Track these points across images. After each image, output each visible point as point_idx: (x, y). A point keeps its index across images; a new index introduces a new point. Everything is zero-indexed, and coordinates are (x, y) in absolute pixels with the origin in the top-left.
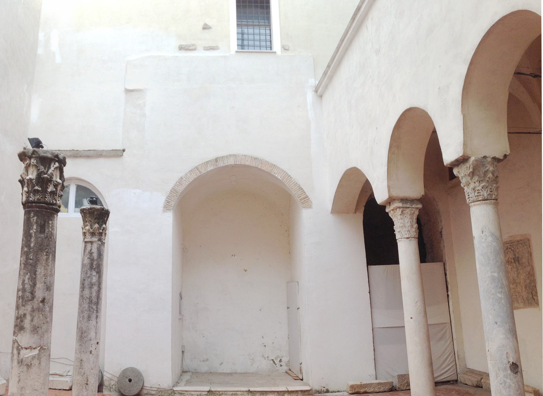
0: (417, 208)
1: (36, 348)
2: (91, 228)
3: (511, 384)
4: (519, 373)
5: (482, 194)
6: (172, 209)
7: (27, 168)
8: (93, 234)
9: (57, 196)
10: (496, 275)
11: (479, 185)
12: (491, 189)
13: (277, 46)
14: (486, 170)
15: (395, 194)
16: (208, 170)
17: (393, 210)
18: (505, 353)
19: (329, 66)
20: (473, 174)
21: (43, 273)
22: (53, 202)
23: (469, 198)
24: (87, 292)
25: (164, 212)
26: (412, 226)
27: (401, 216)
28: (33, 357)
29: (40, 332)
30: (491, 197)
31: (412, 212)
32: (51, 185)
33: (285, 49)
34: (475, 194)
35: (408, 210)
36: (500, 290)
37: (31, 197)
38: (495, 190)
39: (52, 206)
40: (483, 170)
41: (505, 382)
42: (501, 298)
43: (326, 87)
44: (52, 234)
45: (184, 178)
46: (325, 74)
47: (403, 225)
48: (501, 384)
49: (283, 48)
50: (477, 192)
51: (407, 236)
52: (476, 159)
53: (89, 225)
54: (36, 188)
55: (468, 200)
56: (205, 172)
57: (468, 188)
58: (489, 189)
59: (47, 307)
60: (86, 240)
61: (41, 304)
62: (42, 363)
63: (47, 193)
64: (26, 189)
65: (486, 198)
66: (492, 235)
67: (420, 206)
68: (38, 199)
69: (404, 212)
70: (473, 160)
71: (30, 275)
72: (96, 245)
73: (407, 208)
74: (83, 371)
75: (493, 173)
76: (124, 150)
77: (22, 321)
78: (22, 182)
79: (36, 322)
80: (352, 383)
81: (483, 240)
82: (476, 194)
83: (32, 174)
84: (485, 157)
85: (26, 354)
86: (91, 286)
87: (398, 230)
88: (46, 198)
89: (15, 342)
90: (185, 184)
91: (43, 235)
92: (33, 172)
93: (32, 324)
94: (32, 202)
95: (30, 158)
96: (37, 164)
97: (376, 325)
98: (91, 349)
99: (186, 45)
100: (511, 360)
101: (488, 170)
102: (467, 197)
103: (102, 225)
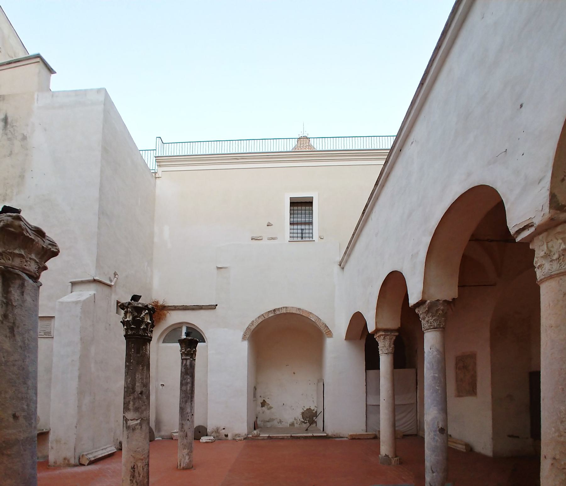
0: (395, 335)
1: (138, 419)
2: (186, 351)
3: (438, 439)
4: (445, 434)
5: (433, 324)
6: (248, 339)
7: (126, 314)
8: (187, 355)
9: (148, 331)
10: (437, 375)
11: (432, 318)
12: (440, 321)
13: (316, 237)
14: (438, 309)
15: (380, 326)
16: (270, 316)
17: (378, 337)
18: (437, 422)
19: (348, 248)
20: (427, 312)
21: (140, 377)
22: (145, 334)
23: (424, 327)
24: (184, 388)
25: (242, 341)
26: (390, 346)
27: (383, 340)
28: (137, 424)
29: (140, 410)
30: (439, 326)
31: (391, 338)
32: (143, 325)
33: (321, 238)
34: (428, 324)
35: (388, 337)
36: (438, 385)
37: (129, 332)
38: (443, 322)
39: (144, 337)
40: (435, 309)
41: (434, 438)
42: (438, 390)
43: (346, 262)
44: (146, 354)
45: (255, 322)
46: (345, 253)
47: (384, 345)
48: (432, 439)
49: (320, 237)
50: (429, 323)
51: (386, 352)
52: (431, 302)
53: (184, 349)
54: (132, 326)
55: (423, 329)
56: (268, 317)
57: (423, 321)
58: (439, 322)
59: (144, 396)
60: (182, 358)
61: (140, 395)
62: (143, 427)
63: (140, 329)
64: (125, 327)
65: (436, 327)
66: (437, 350)
67: (397, 334)
68: (134, 333)
69: (385, 338)
70: (429, 303)
71: (132, 379)
72: (189, 361)
73: (387, 335)
74: (184, 430)
75: (443, 310)
76: (216, 305)
77: (128, 405)
78: (123, 323)
79: (137, 405)
80: (352, 433)
81: (431, 354)
82: (429, 325)
83: (129, 318)
84: (438, 300)
85: (131, 423)
86: (187, 384)
87: (381, 349)
88: (140, 332)
89: (124, 417)
90: (255, 324)
91: (139, 355)
92: (130, 316)
93: (134, 406)
94: (130, 335)
95: (127, 307)
96: (132, 311)
97: (368, 403)
98: (188, 418)
99: (256, 237)
100: (440, 426)
101: (439, 309)
102: (423, 327)
103: (193, 349)
